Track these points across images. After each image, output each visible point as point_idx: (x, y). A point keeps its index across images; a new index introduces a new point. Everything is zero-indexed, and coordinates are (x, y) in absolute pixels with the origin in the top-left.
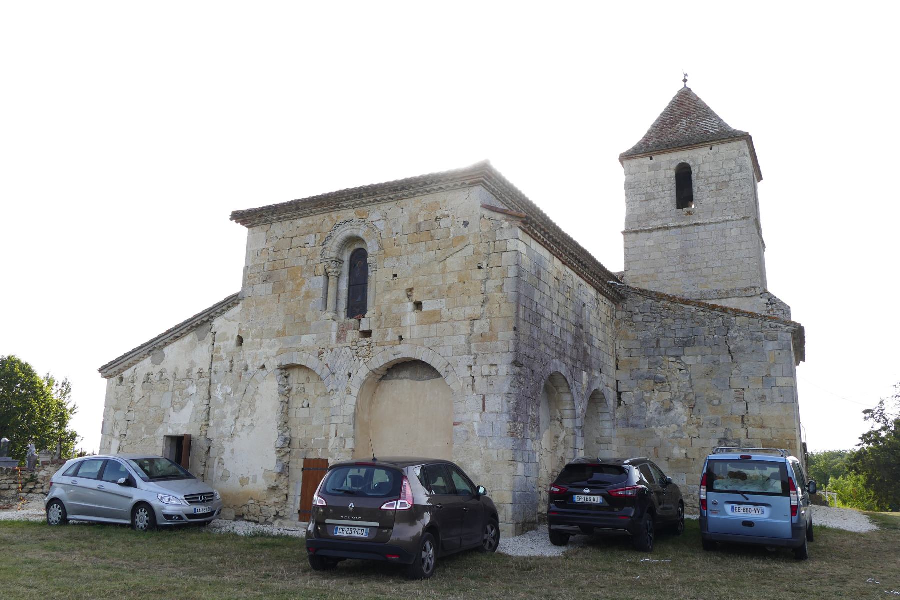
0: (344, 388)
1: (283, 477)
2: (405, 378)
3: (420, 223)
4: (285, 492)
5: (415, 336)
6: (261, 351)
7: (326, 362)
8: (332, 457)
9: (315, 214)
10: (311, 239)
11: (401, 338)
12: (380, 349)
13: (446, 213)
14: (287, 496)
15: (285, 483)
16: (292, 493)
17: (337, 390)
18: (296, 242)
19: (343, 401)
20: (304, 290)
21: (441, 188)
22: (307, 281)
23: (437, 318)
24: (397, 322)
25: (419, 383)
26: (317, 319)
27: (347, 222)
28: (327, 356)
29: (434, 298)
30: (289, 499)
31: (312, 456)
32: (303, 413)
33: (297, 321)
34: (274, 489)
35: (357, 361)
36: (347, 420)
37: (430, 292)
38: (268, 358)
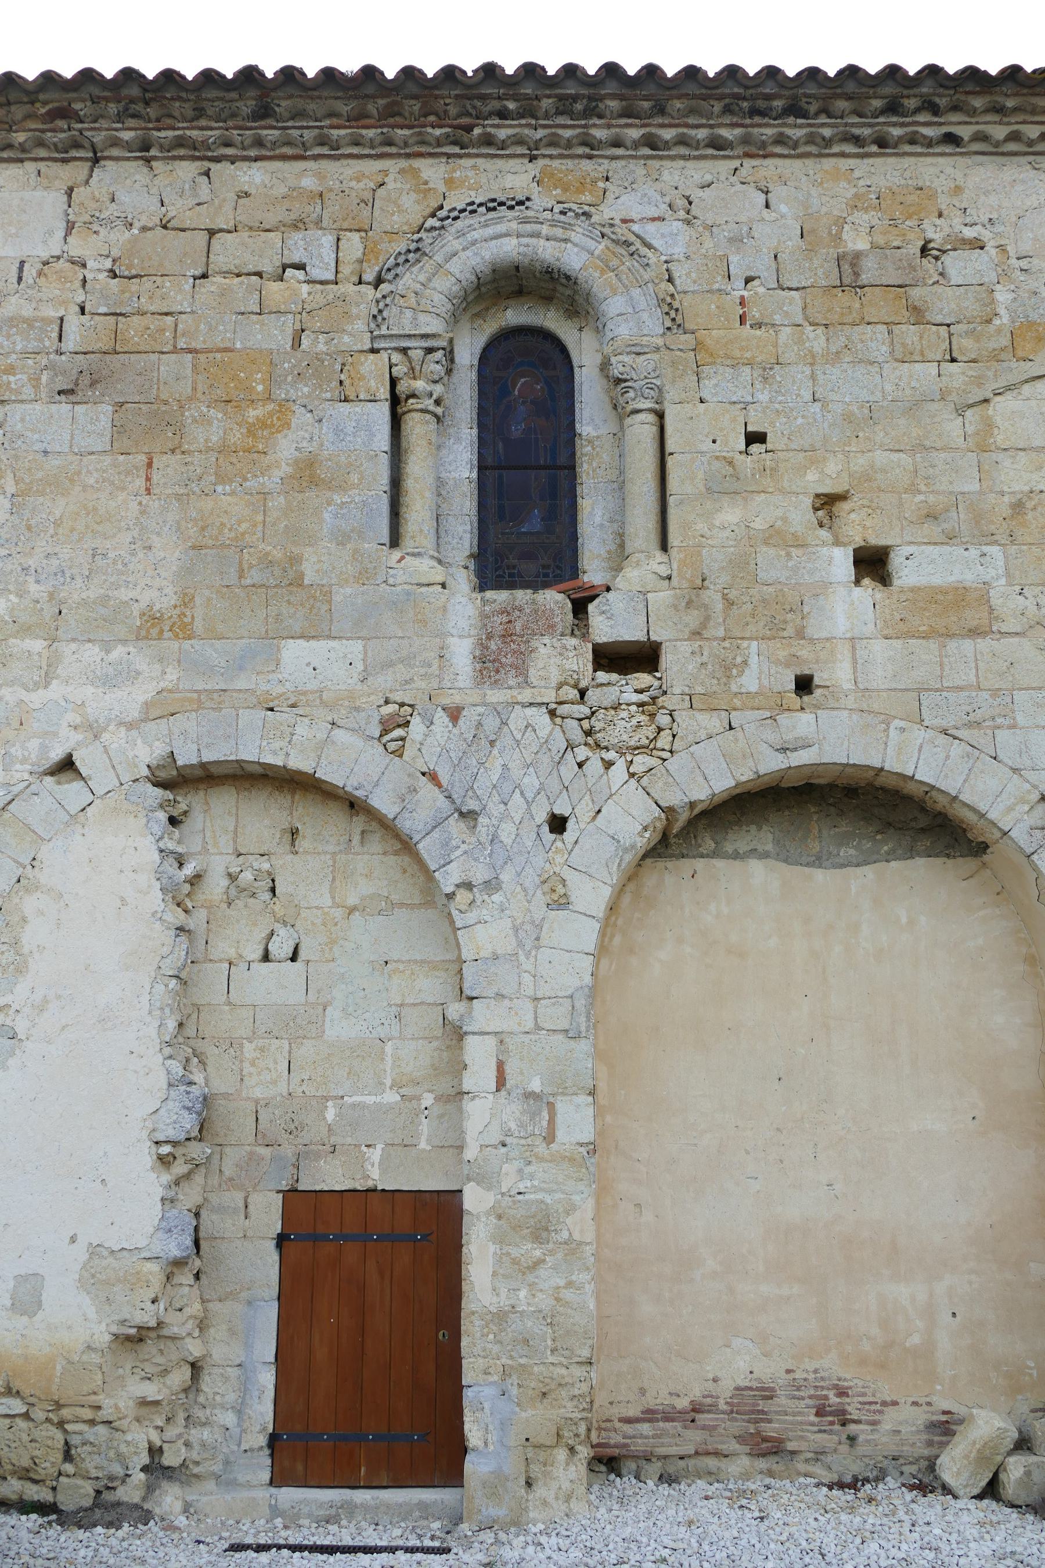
0: (530, 879)
1: (186, 1278)
2: (753, 853)
3: (858, 255)
4: (194, 1349)
5: (879, 677)
6: (56, 690)
7: (430, 760)
8: (483, 1180)
9: (333, 150)
10: (319, 251)
11: (804, 685)
12: (714, 722)
13: (969, 233)
14: (195, 1367)
15: (195, 1308)
16: (221, 1350)
17: (492, 885)
18: (229, 251)
19: (531, 937)
20: (285, 449)
21: (950, 139)
22: (301, 417)
23: (974, 617)
24: (786, 616)
25: (820, 876)
26: (364, 576)
27: (502, 210)
28: (431, 739)
29: (950, 538)
30: (207, 1384)
31: (331, 1176)
32: (274, 986)
33: (254, 576)
34: (134, 1339)
35: (594, 766)
36: (556, 1016)
37: (932, 516)
38: (94, 731)
